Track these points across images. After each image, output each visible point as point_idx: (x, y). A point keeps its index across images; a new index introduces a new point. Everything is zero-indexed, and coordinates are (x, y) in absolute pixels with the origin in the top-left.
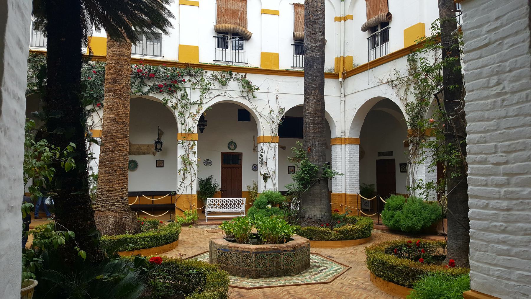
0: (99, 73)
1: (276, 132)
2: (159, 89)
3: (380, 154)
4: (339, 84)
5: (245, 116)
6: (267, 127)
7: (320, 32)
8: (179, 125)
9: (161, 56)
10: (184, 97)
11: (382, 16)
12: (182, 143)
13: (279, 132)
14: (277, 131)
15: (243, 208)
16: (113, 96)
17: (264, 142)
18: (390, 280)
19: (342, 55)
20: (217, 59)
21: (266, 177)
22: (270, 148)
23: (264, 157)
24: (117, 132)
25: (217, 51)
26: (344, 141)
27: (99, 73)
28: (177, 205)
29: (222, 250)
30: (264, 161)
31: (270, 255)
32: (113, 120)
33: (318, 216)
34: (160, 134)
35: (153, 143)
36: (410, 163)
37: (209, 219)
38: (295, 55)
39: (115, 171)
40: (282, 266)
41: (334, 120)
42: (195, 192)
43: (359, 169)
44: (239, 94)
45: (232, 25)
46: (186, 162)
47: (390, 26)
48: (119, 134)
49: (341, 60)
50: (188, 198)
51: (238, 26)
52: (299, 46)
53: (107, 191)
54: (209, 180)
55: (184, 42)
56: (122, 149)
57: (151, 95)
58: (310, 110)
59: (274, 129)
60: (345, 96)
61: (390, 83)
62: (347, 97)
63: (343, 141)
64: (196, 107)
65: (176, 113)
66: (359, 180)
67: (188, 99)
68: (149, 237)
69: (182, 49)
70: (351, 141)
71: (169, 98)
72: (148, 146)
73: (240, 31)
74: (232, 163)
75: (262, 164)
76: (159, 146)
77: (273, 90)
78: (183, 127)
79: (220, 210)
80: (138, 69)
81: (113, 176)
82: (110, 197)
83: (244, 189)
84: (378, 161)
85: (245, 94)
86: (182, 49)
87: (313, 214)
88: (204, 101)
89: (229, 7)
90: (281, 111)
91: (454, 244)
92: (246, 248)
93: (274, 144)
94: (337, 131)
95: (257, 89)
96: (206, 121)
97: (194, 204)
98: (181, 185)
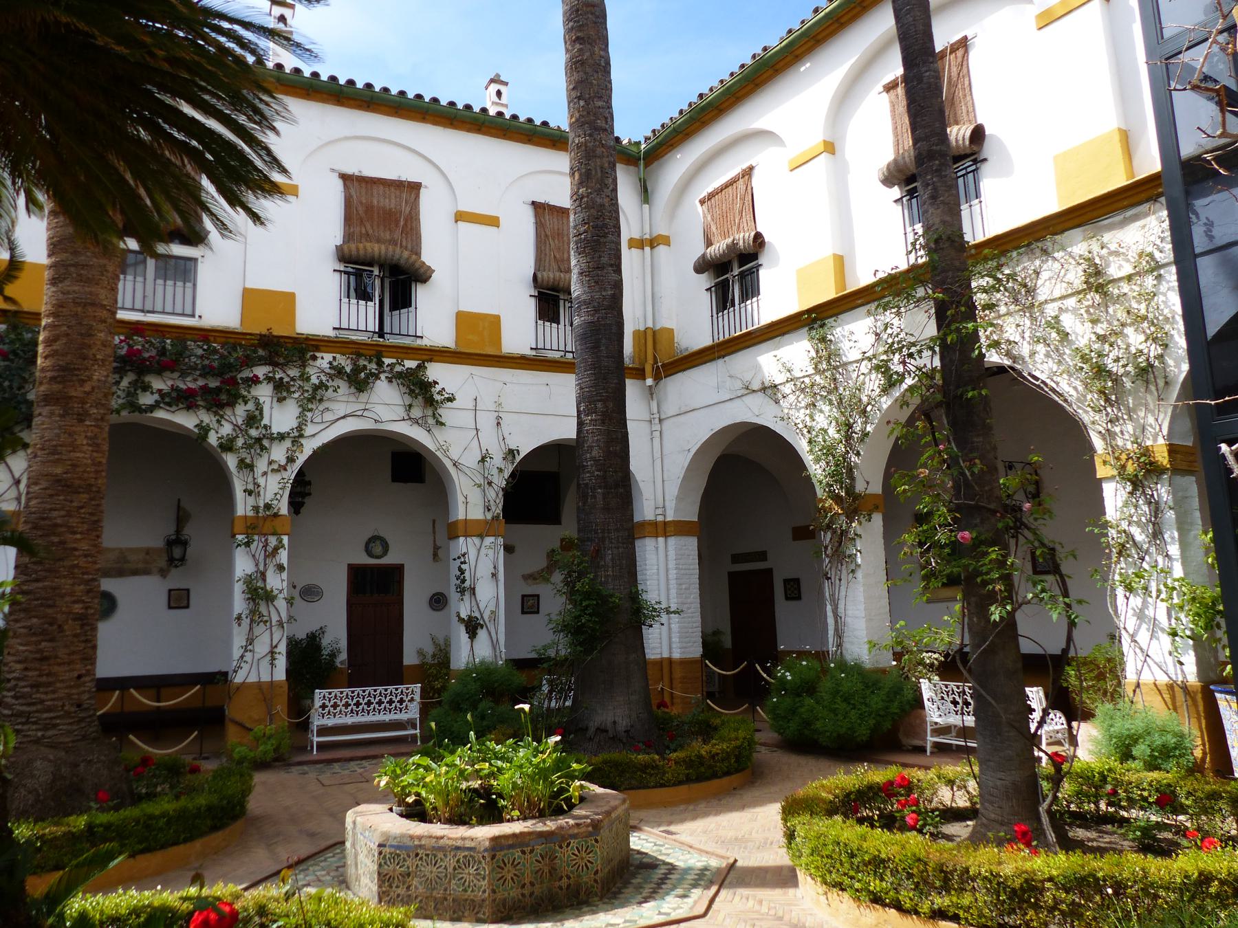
0: (16, 355)
1: (498, 510)
2: (185, 400)
3: (736, 559)
4: (647, 392)
5: (411, 467)
6: (472, 499)
7: (611, 265)
8: (239, 494)
9: (193, 316)
10: (253, 419)
11: (743, 237)
12: (248, 544)
13: (504, 510)
14: (500, 506)
15: (413, 712)
16: (61, 416)
17: (466, 536)
18: (877, 900)
20: (345, 325)
21: (473, 626)
22: (483, 551)
23: (467, 574)
24: (69, 515)
25: (345, 307)
27: (16, 355)
28: (232, 712)
29: (391, 846)
30: (467, 584)
31: (532, 851)
32: (58, 480)
33: (623, 724)
34: (182, 518)
36: (828, 579)
37: (321, 746)
38: (540, 322)
39: (60, 626)
40: (565, 880)
42: (280, 674)
43: (700, 595)
44: (401, 412)
45: (383, 247)
46: (258, 594)
47: (760, 261)
48: (73, 521)
50: (264, 691)
51: (398, 250)
52: (549, 301)
53: (32, 686)
54: (313, 640)
55: (254, 283)
56: (82, 562)
57: (161, 414)
58: (595, 453)
59: (492, 503)
60: (660, 420)
61: (769, 392)
62: (666, 424)
63: (660, 530)
64: (288, 443)
65: (231, 461)
66: (699, 624)
67: (265, 427)
68: (163, 815)
69: (251, 298)
71: (214, 425)
72: (148, 551)
73: (402, 262)
74: (375, 590)
75: (462, 592)
76: (177, 552)
77: (487, 403)
78: (251, 501)
79: (349, 720)
80: (130, 347)
81: (52, 640)
82: (42, 702)
83: (410, 658)
84: (731, 575)
85: (417, 413)
86: (251, 298)
87: (610, 719)
88: (309, 430)
89: (375, 202)
90: (510, 458)
91: (999, 783)
92: (463, 839)
93: (492, 539)
94: (645, 503)
95: (451, 400)
96: (309, 483)
97: (279, 708)
98: (242, 657)
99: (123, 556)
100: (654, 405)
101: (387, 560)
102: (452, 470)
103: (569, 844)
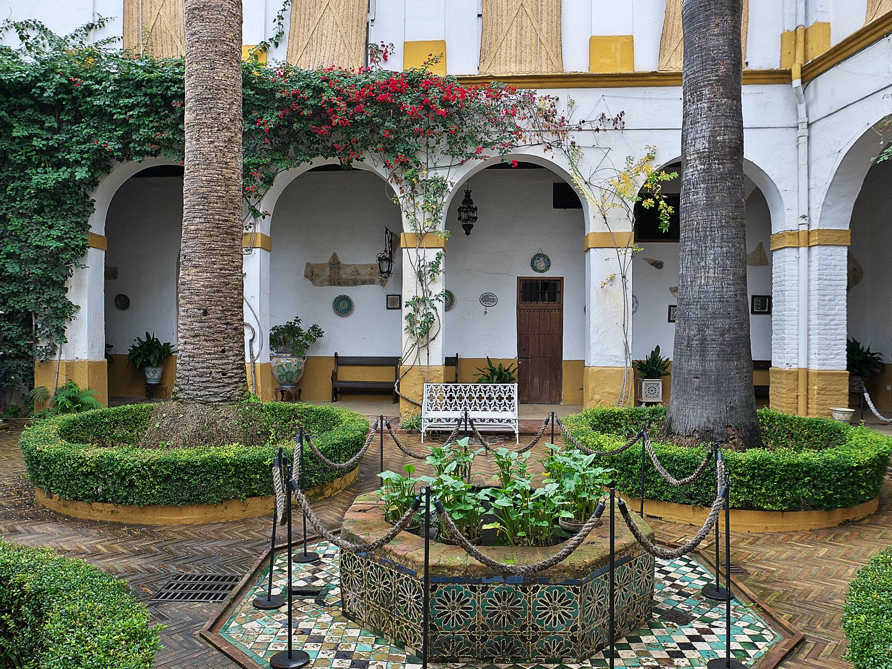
6: (608, 214)
19: (801, 21)
26: (806, 239)
35: (375, 261)
41: (780, 187)
49: (798, 36)
60: (809, 125)
70: (827, 239)
94: (787, 213)
99: (356, 270)
100: (802, 108)
101: (547, 274)
102: (584, 187)
103: (536, 589)
